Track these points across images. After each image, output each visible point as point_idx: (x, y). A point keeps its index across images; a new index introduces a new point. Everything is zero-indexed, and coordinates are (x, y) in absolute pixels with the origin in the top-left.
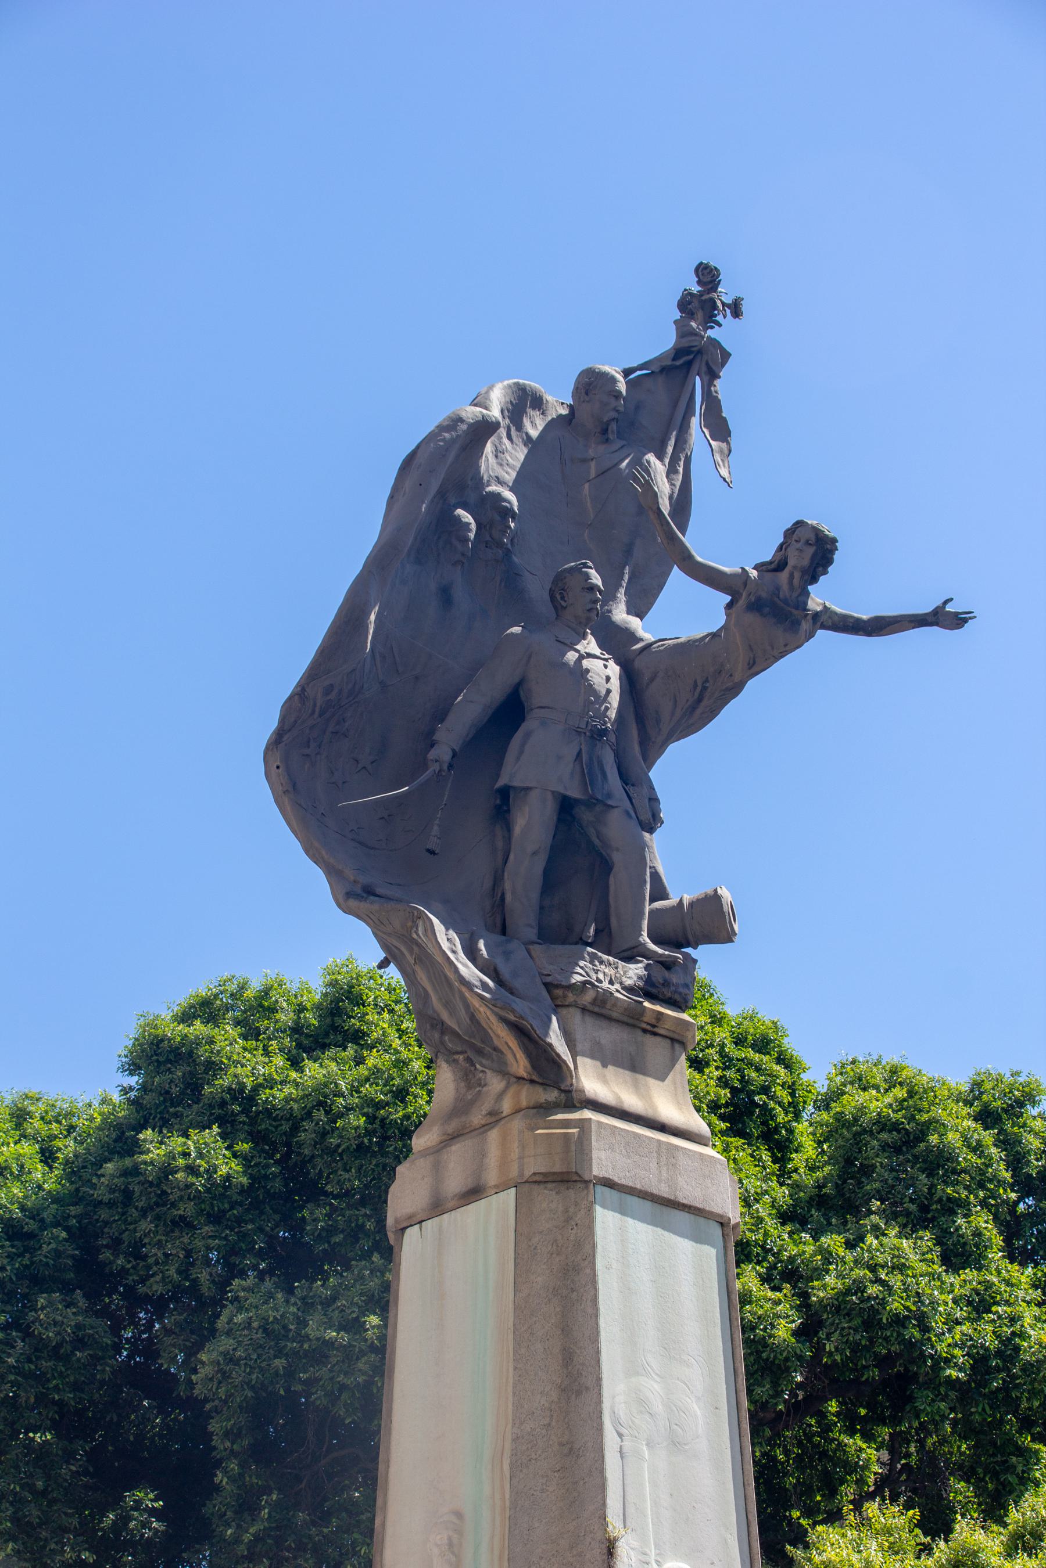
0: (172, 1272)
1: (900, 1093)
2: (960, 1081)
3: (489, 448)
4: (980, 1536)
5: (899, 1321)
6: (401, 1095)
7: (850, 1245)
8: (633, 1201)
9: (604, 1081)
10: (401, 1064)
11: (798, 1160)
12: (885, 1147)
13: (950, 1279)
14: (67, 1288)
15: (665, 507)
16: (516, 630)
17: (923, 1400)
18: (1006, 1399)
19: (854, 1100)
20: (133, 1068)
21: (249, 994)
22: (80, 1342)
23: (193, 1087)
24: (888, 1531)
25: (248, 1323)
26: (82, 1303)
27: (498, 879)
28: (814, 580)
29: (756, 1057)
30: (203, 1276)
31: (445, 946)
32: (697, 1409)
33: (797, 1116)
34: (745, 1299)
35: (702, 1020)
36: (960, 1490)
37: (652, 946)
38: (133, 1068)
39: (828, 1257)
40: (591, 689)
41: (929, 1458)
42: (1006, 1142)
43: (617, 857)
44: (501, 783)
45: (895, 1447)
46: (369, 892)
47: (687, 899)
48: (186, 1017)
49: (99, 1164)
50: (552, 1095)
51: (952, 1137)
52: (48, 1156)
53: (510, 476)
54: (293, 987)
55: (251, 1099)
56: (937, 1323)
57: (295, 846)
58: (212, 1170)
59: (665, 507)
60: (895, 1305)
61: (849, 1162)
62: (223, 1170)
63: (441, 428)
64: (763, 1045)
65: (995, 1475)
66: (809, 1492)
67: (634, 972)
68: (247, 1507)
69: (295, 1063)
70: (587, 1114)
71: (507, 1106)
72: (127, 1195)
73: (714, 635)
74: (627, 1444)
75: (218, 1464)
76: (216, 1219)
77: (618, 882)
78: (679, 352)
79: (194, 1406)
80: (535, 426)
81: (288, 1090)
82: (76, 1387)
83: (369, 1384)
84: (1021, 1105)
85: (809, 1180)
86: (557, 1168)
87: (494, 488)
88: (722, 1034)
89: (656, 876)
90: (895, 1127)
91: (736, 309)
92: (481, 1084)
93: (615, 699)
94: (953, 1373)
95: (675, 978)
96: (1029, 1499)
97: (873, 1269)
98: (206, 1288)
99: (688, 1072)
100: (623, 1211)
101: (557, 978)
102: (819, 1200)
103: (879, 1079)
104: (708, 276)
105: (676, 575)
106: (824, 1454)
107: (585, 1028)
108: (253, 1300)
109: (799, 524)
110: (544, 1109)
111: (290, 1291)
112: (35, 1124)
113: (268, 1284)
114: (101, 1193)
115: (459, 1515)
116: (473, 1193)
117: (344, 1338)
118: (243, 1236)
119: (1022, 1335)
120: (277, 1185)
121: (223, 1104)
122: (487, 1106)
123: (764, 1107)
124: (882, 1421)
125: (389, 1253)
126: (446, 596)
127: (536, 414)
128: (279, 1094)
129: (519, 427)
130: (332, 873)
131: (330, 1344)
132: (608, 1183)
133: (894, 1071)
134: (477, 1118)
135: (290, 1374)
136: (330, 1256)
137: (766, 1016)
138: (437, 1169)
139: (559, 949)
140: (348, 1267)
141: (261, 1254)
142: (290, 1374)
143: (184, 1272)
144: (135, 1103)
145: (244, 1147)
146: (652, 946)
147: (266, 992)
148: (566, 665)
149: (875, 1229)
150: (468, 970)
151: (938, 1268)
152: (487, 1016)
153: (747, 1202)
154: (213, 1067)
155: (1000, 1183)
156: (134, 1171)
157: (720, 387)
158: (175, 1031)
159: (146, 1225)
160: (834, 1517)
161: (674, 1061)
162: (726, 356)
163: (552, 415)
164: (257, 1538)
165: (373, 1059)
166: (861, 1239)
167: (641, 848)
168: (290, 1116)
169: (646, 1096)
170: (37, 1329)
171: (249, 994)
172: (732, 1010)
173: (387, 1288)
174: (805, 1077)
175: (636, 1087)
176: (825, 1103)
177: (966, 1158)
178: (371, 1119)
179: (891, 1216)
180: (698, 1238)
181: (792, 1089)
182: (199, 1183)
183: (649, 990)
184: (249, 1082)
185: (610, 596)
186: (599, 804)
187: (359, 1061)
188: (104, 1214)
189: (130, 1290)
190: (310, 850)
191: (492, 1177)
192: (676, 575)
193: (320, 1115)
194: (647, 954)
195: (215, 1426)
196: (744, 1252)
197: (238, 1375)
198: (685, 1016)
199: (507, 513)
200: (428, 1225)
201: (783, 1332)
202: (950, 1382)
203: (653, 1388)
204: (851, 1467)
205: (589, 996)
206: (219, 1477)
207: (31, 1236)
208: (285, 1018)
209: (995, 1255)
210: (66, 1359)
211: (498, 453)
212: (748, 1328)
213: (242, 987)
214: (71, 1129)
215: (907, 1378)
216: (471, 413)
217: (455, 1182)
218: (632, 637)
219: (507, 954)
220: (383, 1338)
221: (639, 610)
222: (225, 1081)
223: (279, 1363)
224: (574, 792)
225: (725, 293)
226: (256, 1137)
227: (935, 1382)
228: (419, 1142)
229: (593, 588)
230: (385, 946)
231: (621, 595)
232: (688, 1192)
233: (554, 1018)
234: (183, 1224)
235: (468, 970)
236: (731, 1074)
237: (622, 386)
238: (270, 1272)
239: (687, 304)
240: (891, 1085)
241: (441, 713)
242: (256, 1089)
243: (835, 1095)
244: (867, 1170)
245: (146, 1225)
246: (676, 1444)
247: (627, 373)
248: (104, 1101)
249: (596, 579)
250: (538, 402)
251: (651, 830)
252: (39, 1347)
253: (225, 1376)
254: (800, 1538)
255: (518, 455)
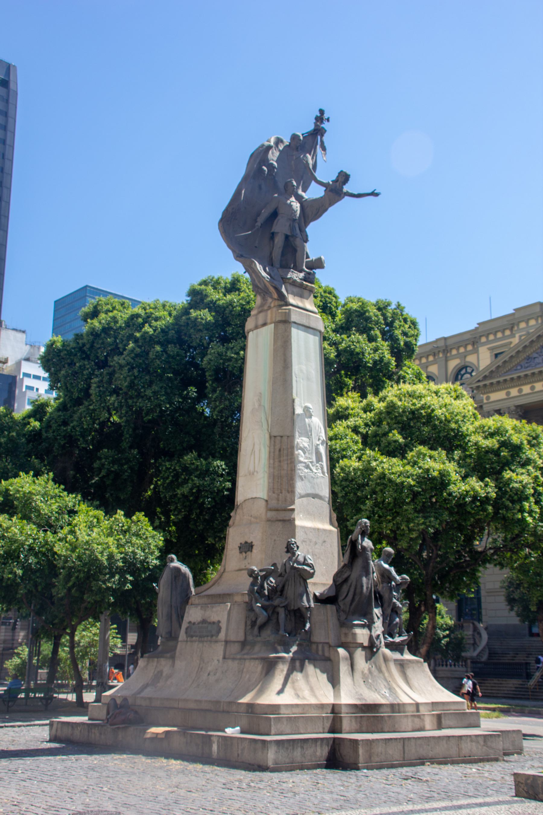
0: (198, 341)
1: (360, 304)
2: (374, 301)
3: (270, 152)
4: (373, 399)
5: (358, 354)
6: (248, 303)
7: (348, 337)
8: (300, 327)
9: (294, 299)
10: (248, 296)
11: (337, 319)
12: (356, 316)
13: (369, 344)
14: (175, 344)
15: (311, 167)
16: (276, 195)
17: (362, 370)
18: (380, 370)
19: (350, 305)
20: (189, 295)
21: (214, 279)
22: (178, 355)
23: (202, 300)
24: (353, 398)
25: (214, 353)
26: (178, 347)
27: (271, 253)
28: (345, 184)
29: (328, 295)
30: (205, 342)
31: (259, 268)
32: (313, 372)
33: (337, 309)
34: (325, 349)
35: (317, 287)
36: (369, 389)
37: (306, 269)
38: (189, 295)
39: (343, 340)
40: (293, 210)
41: (363, 383)
42: (384, 315)
43: (298, 249)
44: (272, 231)
45: (356, 381)
46: (241, 256)
47: (314, 258)
48: (200, 284)
49: (181, 317)
50: (283, 303)
51: (371, 314)
52: (170, 315)
53: (275, 159)
54: (224, 278)
55: (215, 303)
56: (366, 355)
57: (224, 245)
58: (206, 319)
59: (311, 167)
60: (358, 350)
61: (348, 319)
62: (209, 319)
63: (260, 147)
64: (330, 293)
65: (377, 386)
66: (337, 390)
67: (302, 275)
68: (214, 391)
69: (225, 295)
70: (290, 307)
71: (272, 305)
72: (188, 324)
73: (322, 197)
74: (298, 379)
75: (207, 382)
76: (207, 329)
77: (298, 254)
78: (315, 130)
79: (203, 370)
80: (281, 147)
81: (223, 301)
82: (177, 365)
83: (241, 366)
84: (387, 306)
85: (340, 323)
86: (284, 319)
87: (271, 162)
88: (321, 290)
89: (307, 253)
90: (359, 311)
91: (328, 120)
92: (267, 300)
93: (298, 212)
94: (369, 365)
95: (311, 277)
96: (384, 391)
97: (353, 342)
98: (205, 345)
99: (313, 299)
100: (298, 329)
101: (285, 276)
102: (342, 327)
103: (356, 301)
104: (322, 112)
105: (313, 183)
106: (340, 382)
107: (290, 288)
108: (215, 347)
109: (342, 171)
110: (281, 306)
111: (224, 346)
112: (167, 308)
113: (219, 344)
114: (182, 323)
115: (261, 393)
116: (265, 324)
117: (235, 356)
118: (214, 333)
119: (384, 357)
120: (221, 322)
121: (209, 304)
122: (268, 305)
123: (330, 307)
124: (353, 375)
125: (245, 337)
126: (260, 187)
127: (281, 144)
128: (221, 302)
129: (277, 147)
130: (234, 252)
131: (232, 357)
132: (295, 323)
133: (359, 299)
134: (266, 308)
135: (224, 363)
136: (233, 339)
137: (331, 286)
138: (257, 319)
139: (285, 270)
140: (236, 341)
141: (217, 338)
142: (224, 363)
143: (200, 341)
144: (189, 304)
145: (213, 314)
146: (306, 269)
147: (218, 279)
148: (287, 204)
149: (354, 334)
150: (264, 274)
151: (367, 342)
152: (268, 285)
153: (325, 328)
154: (206, 296)
155: (381, 324)
156: (189, 319)
157: (325, 138)
158: (198, 288)
159: (192, 331)
160: (342, 395)
161: (310, 296)
162: (326, 131)
163: (285, 144)
164: (216, 397)
165: (242, 295)
166: (350, 336)
167: (303, 247)
168: (224, 307)
169: (304, 304)
170: (169, 352)
171: (214, 279)
172: (323, 285)
173: (245, 345)
174: (339, 300)
175: (302, 302)
176: (343, 306)
177: (374, 318)
178: (242, 308)
179: (357, 331)
180: (315, 335)
181: (336, 302)
182: (204, 322)
183: (305, 279)
184: (214, 299)
185: (298, 187)
186: (294, 236)
187: (239, 295)
188: (183, 328)
189: (189, 345)
190: (229, 246)
191: (269, 321)
192: (313, 183)
193: (230, 307)
194: (305, 271)
195: (207, 374)
196: (325, 339)
197: (212, 363)
198: (313, 286)
199: (274, 167)
200: (255, 331)
201: (332, 356)
202: (368, 367)
203: (304, 367)
204: (346, 385)
205: (291, 281)
206: (207, 384)
207: (167, 332)
208: (223, 285)
209: (379, 339)
210: (175, 359)
211: (273, 153)
212: (325, 355)
213: (213, 278)
214: (175, 309)
215: (359, 366)
216: (267, 144)
217: (260, 322)
218: (303, 198)
219: (273, 271)
220: (244, 356)
221: (304, 190)
222: (209, 299)
223: (221, 361)
224: (289, 234)
225: (326, 116)
226: (216, 312)
227: (365, 367)
228: (253, 313)
229: (294, 186)
230: (245, 268)
231: (300, 187)
232: (313, 325)
233: (283, 286)
234: (200, 330)
235: (264, 274)
236: (323, 299)
237: (301, 138)
238: (219, 341)
239: (317, 119)
240: (358, 302)
241: (259, 214)
242: (216, 301)
243: (346, 304)
244: (352, 321)
245: (192, 331)
246: (308, 379)
247: (303, 135)
248: (183, 303)
249: (295, 183)
250: (282, 141)
251: (306, 242)
252: (169, 356)
253: (209, 363)
254: (334, 399)
255: (277, 154)
